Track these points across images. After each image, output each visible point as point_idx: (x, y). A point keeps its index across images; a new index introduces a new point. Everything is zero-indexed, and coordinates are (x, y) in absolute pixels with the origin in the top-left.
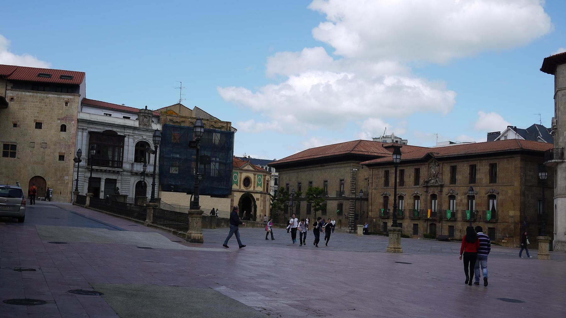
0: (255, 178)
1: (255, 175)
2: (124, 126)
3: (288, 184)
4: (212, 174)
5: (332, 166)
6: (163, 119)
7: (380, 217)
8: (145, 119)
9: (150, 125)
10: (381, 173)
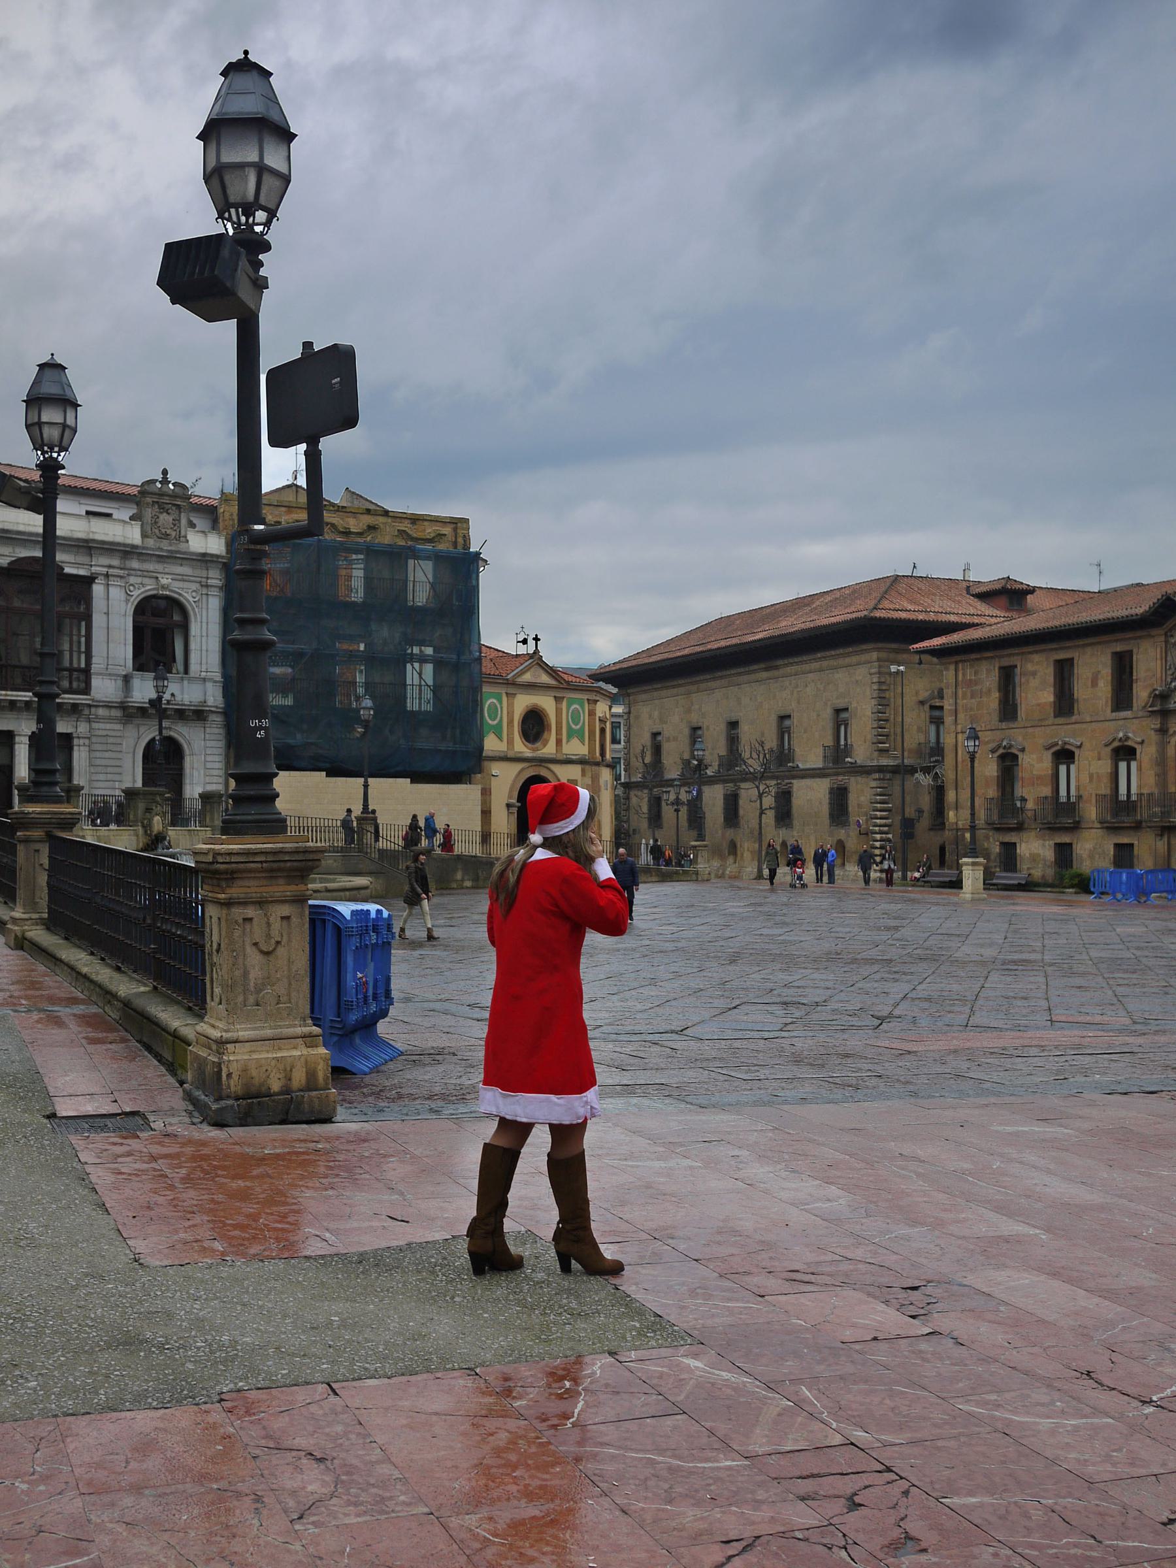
0: (559, 712)
1: (558, 700)
2: (86, 541)
3: (659, 734)
4: (412, 704)
5: (806, 667)
6: (227, 515)
7: (1101, 823)
8: (165, 519)
9: (181, 538)
10: (987, 675)
